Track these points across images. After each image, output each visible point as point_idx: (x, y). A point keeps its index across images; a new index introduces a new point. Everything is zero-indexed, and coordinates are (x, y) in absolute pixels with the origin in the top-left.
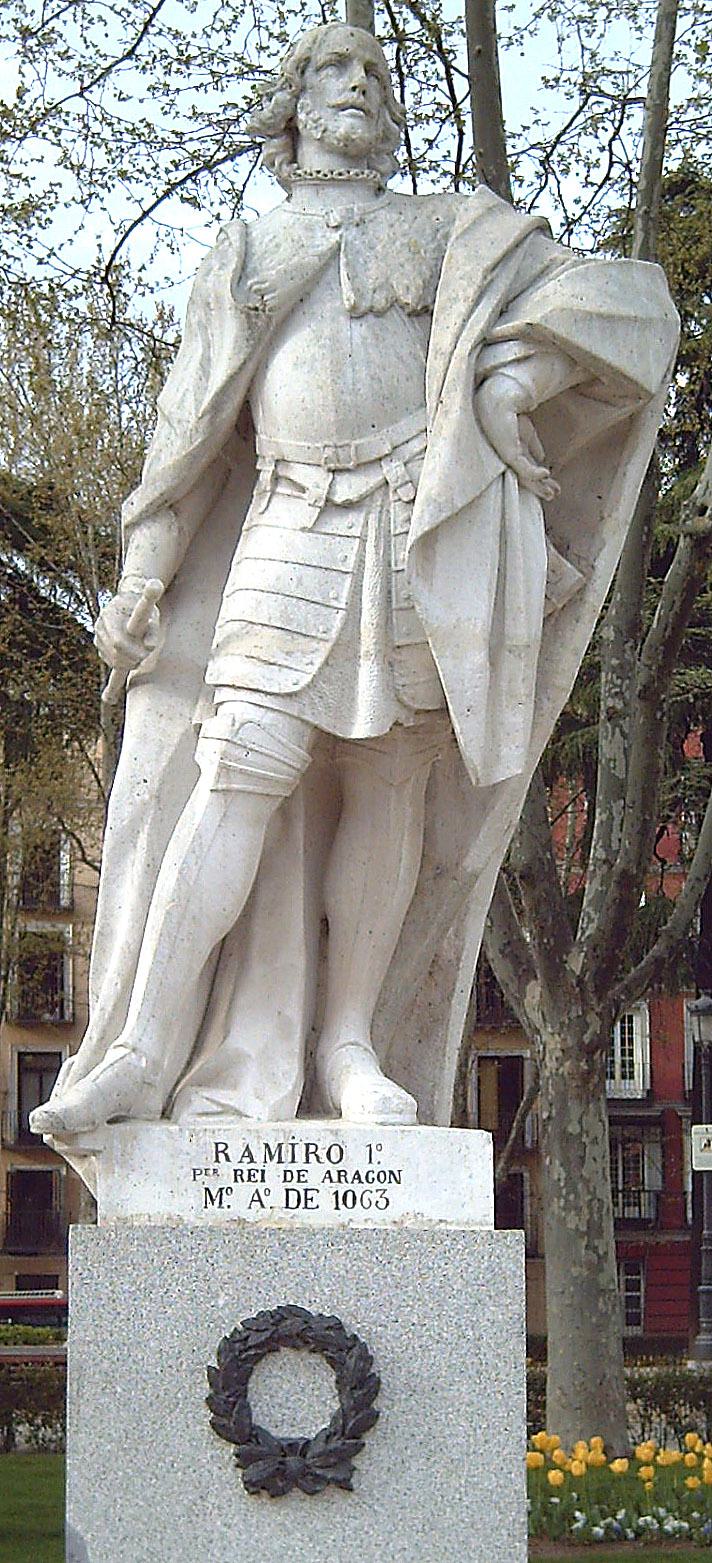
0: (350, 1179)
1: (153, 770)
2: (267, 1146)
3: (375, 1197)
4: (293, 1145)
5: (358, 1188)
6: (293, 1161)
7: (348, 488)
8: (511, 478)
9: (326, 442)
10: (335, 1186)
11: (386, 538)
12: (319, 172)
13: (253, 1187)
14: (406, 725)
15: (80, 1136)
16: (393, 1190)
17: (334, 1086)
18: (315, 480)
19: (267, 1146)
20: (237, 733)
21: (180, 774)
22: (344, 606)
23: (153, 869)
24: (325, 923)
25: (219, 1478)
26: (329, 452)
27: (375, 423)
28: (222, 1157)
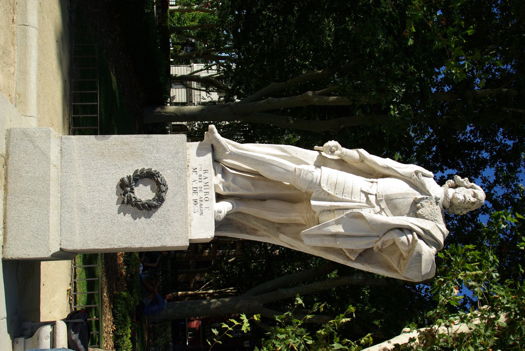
0: (200, 203)
1: (299, 156)
2: (208, 183)
3: (196, 209)
5: (198, 205)
6: (204, 189)
8: (378, 239)
10: (198, 199)
11: (361, 207)
13: (198, 179)
16: (198, 214)
19: (208, 183)
21: (300, 162)
24: (265, 200)
25: (124, 172)
26: (381, 193)
27: (389, 204)
28: (205, 172)
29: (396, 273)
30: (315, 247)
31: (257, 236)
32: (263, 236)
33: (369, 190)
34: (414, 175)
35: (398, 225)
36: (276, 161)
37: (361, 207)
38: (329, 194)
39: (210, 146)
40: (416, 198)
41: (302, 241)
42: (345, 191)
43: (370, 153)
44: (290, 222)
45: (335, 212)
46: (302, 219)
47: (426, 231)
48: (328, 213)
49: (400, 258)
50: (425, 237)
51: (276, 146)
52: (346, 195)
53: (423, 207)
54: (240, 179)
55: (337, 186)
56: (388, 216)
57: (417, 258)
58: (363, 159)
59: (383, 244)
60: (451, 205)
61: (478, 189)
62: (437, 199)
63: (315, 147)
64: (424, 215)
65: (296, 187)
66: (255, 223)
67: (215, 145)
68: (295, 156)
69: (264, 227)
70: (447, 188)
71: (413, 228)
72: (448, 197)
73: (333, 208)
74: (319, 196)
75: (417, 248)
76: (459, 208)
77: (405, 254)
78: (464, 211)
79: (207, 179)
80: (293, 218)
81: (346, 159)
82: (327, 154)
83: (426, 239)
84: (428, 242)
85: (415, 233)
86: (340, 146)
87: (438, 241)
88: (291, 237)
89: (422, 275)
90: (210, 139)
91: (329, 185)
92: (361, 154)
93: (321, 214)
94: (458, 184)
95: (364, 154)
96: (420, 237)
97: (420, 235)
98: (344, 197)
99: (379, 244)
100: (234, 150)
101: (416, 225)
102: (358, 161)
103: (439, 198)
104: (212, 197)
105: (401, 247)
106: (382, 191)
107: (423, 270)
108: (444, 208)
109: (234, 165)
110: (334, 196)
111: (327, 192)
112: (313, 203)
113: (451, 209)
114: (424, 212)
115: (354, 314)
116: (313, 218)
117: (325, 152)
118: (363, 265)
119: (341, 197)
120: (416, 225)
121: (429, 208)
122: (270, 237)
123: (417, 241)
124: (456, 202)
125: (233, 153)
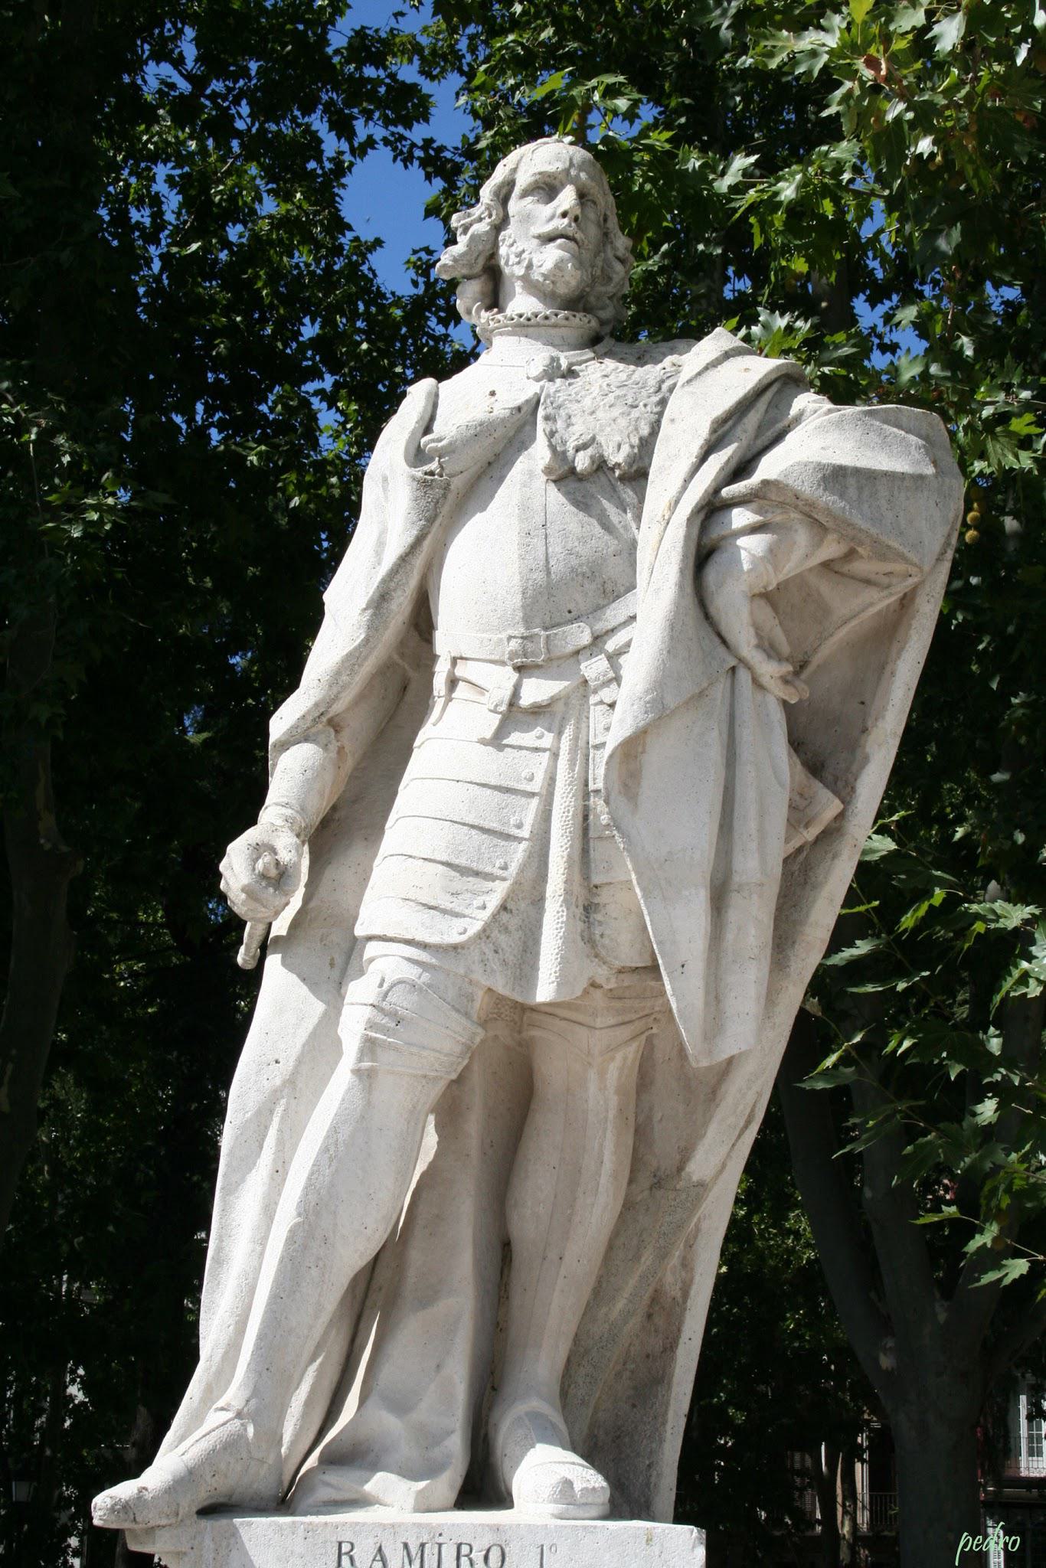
2: (406, 1546)
4: (440, 1545)
7: (536, 691)
8: (743, 676)
9: (510, 632)
11: (583, 752)
12: (521, 316)
14: (607, 987)
15: (158, 1532)
17: (507, 1464)
18: (500, 681)
19: (406, 1546)
20: (386, 995)
22: (527, 836)
23: (279, 1173)
26: (514, 644)
29: (918, 601)
30: (770, 998)
31: (686, 1294)
32: (686, 1264)
33: (495, 700)
34: (432, 473)
35: (682, 571)
36: (312, 1173)
37: (583, 752)
38: (504, 908)
39: (207, 1524)
40: (548, 470)
41: (730, 1061)
42: (494, 825)
43: (294, 685)
44: (632, 1119)
45: (596, 879)
46: (619, 1056)
47: (715, 436)
48: (599, 917)
49: (842, 575)
50: (745, 443)
51: (227, 1165)
52: (512, 822)
53: (593, 439)
54: (387, 1373)
55: (462, 861)
56: (633, 618)
57: (852, 492)
58: (324, 719)
59: (770, 649)
60: (581, 306)
61: (514, 170)
62: (553, 372)
63: (240, 960)
64: (635, 441)
65: (454, 1076)
66: (620, 1304)
67: (202, 1497)
68: (288, 1065)
69: (647, 1258)
70: (499, 317)
71: (702, 498)
72: (546, 318)
73: (577, 889)
74: (510, 959)
75: (807, 486)
76: (602, 271)
77: (831, 549)
78: (615, 249)
79: (386, 1551)
80: (614, 1101)
81: (318, 807)
82: (287, 904)
83: (756, 437)
84: (770, 434)
85: (725, 492)
86: (250, 836)
87: (766, 382)
88: (706, 1124)
89: (936, 476)
90: (173, 1520)
91: (456, 905)
92: (295, 727)
93: (603, 953)
94: (481, 262)
95: (298, 716)
96: (741, 469)
97: (733, 464)
98: (525, 833)
99: (769, 670)
100: (235, 1394)
101: (687, 481)
102: (334, 746)
103: (547, 362)
104: (482, 1525)
105: (791, 566)
106: (504, 636)
107: (899, 465)
108: (593, 341)
109: (308, 1403)
110: (517, 883)
111: (495, 917)
112: (545, 991)
113: (603, 308)
114: (618, 438)
115: (925, 907)
116: (620, 998)
117: (277, 914)
118: (866, 760)
119: (524, 845)
120: (687, 481)
121: (600, 414)
122: (698, 1229)
123: (765, 483)
124: (572, 279)
125: (253, 1402)
